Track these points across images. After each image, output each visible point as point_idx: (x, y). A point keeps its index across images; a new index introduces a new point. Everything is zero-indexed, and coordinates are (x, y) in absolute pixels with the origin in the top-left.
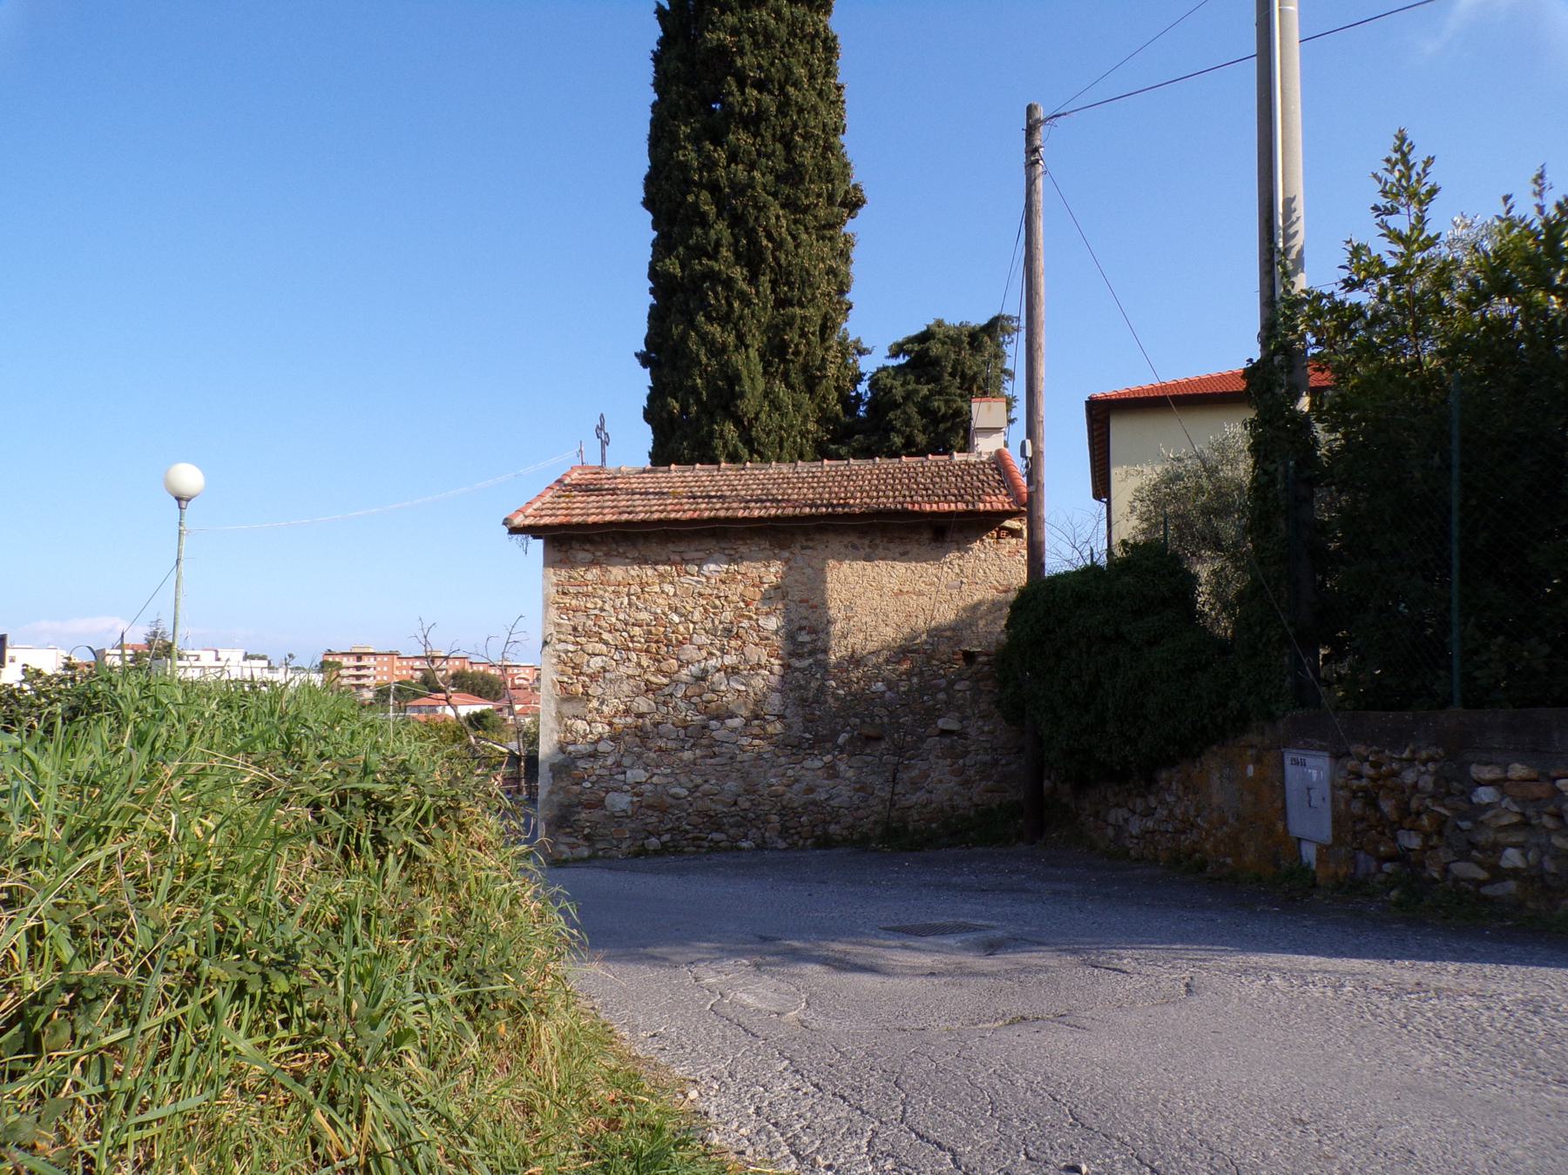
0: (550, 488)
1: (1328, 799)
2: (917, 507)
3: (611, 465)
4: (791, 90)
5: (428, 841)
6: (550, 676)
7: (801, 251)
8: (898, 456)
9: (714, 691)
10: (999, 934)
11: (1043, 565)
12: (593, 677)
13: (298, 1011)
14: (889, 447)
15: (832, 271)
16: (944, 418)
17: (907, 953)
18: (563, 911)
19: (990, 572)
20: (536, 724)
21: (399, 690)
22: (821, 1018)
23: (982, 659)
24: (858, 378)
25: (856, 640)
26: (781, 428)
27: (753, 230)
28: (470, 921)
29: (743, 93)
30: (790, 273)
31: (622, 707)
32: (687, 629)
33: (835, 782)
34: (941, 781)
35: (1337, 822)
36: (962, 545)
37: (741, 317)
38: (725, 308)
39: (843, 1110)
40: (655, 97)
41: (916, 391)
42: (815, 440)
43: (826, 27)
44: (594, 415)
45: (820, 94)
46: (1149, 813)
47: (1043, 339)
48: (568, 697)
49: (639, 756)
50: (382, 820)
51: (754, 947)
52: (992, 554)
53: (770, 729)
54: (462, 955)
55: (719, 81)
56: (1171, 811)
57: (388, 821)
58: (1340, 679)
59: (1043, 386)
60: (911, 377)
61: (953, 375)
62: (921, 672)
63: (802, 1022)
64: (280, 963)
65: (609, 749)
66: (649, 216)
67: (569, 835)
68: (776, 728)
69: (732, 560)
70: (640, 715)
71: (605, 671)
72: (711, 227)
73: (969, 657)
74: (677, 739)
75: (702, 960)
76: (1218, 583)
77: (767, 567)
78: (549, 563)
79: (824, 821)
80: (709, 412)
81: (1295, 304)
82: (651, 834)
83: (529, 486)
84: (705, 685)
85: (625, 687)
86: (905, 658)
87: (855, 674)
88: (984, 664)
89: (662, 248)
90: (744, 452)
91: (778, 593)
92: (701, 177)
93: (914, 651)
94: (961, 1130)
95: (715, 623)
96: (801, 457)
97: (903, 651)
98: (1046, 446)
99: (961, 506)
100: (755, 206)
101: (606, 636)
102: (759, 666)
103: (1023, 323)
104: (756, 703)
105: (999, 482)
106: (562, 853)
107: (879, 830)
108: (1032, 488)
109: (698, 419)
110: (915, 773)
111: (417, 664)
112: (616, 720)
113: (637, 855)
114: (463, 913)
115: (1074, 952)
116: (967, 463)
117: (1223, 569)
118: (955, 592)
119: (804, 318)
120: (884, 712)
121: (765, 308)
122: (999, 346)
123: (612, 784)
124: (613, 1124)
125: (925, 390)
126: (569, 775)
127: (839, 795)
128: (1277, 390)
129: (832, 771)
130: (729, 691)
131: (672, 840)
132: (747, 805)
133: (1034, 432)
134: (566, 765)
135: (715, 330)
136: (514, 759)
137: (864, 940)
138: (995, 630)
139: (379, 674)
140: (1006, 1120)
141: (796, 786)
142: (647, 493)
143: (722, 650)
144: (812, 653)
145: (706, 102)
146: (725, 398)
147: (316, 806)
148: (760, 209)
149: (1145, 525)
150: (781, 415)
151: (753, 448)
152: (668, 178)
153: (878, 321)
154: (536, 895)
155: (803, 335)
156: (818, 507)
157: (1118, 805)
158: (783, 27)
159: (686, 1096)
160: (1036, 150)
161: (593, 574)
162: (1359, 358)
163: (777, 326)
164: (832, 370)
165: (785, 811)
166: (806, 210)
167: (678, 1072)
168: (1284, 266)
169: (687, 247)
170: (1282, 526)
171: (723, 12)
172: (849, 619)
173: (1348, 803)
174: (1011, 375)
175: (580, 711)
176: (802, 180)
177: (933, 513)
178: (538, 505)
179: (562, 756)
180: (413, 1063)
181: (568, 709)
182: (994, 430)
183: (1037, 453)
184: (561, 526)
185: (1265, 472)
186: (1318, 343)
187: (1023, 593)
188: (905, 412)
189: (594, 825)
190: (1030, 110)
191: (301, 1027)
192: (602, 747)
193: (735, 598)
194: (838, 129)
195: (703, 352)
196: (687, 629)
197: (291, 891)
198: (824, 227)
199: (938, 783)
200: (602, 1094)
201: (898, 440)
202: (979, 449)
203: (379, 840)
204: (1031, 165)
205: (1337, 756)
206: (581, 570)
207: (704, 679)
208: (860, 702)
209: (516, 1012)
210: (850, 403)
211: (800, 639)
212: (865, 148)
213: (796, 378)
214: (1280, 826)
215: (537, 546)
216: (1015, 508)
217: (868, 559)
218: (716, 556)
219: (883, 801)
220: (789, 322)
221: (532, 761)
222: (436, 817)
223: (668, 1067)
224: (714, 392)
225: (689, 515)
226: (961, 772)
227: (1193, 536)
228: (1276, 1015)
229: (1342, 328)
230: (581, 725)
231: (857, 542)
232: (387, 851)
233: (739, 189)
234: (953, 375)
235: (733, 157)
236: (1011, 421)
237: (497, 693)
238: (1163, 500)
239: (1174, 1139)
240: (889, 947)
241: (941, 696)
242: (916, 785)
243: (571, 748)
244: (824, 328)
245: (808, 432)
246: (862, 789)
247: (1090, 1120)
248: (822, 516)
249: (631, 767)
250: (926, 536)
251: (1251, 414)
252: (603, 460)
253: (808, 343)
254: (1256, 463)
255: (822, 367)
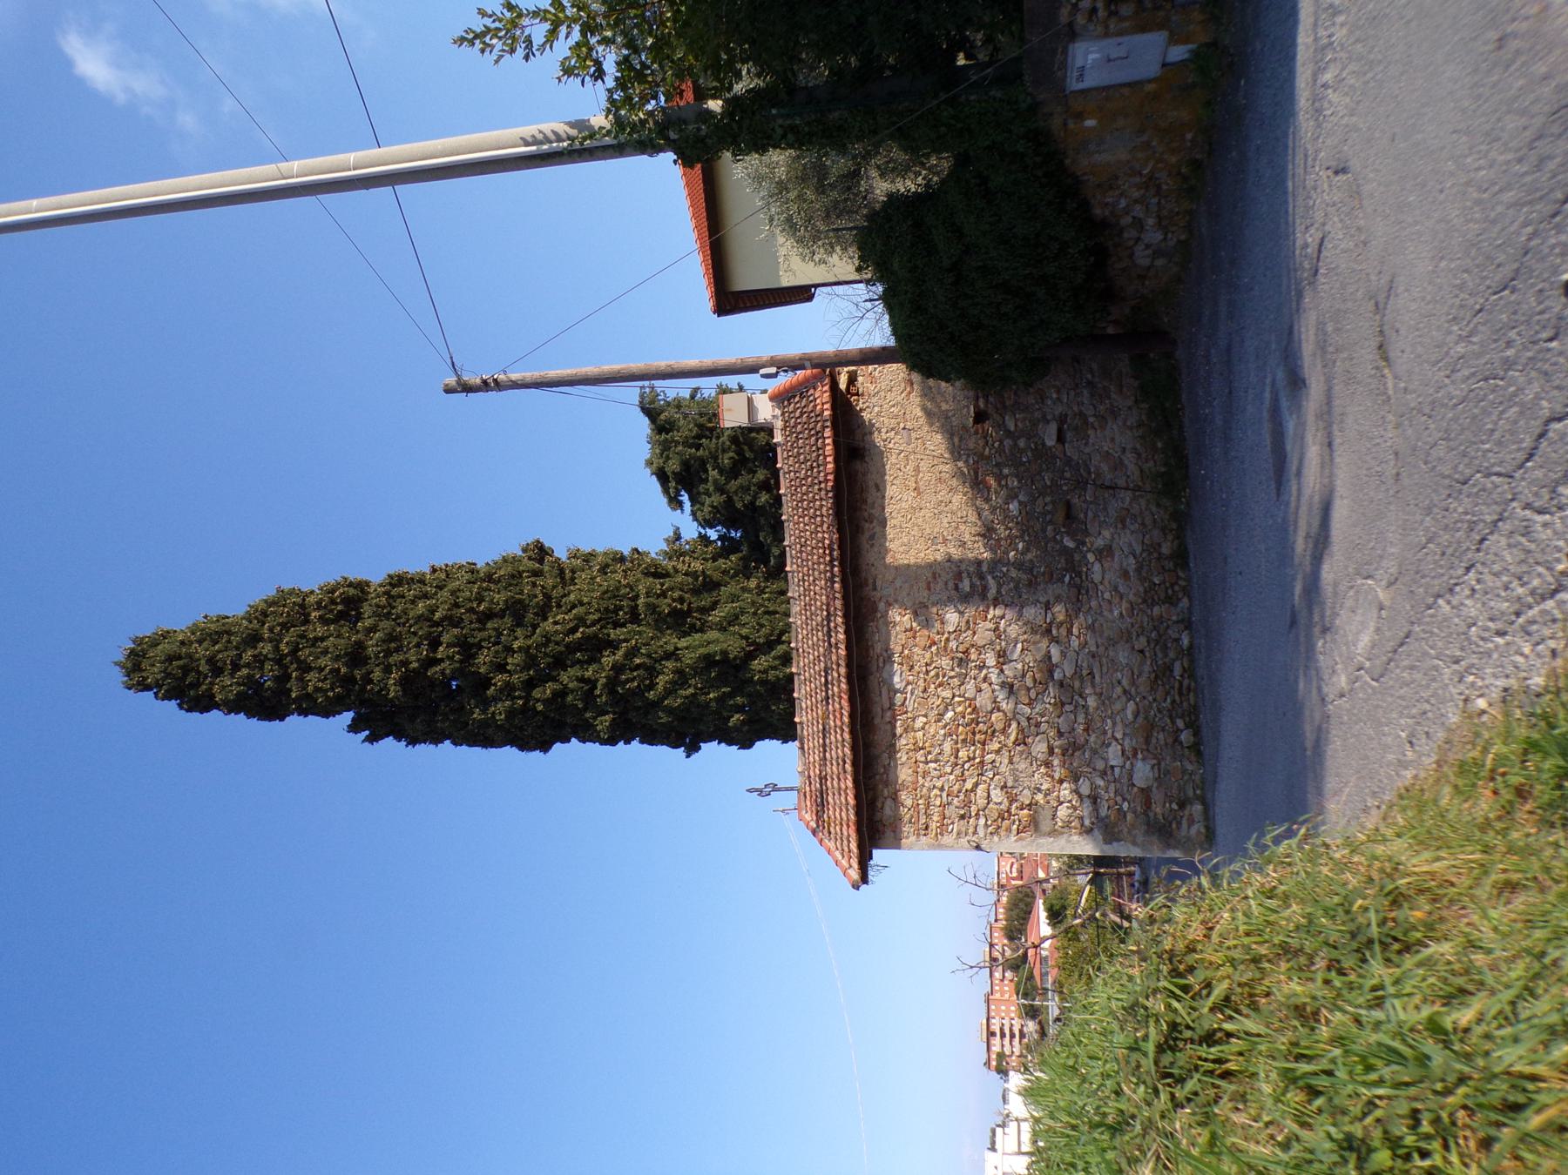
0: (821, 841)
1: (1120, 39)
2: (831, 477)
3: (797, 781)
4: (438, 615)
5: (1208, 985)
6: (1011, 843)
7: (586, 600)
8: (779, 497)
9: (1024, 676)
10: (1281, 374)
11: (884, 349)
12: (1012, 800)
13: (1410, 1140)
14: (771, 506)
15: (603, 570)
16: (740, 453)
17: (1305, 472)
18: (1277, 841)
19: (893, 402)
20: (1058, 857)
21: (1025, 996)
22: (1384, 563)
23: (981, 404)
24: (704, 539)
25: (967, 532)
26: (755, 614)
27: (567, 646)
28: (1295, 943)
29: (442, 660)
30: (606, 609)
31: (1043, 770)
32: (959, 703)
33: (1115, 550)
34: (1113, 440)
35: (1143, 29)
36: (866, 430)
37: (649, 656)
38: (641, 672)
39: (1497, 541)
40: (447, 742)
41: (715, 482)
42: (766, 580)
43: (381, 585)
44: (747, 799)
45: (440, 588)
46: (1139, 224)
47: (662, 364)
48: (1033, 825)
49: (1094, 752)
50: (1188, 1034)
51: (1303, 634)
52: (874, 400)
53: (1061, 617)
54: (1335, 954)
55: (432, 683)
56: (1136, 201)
57: (1188, 1027)
58: (988, 40)
59: (708, 361)
60: (702, 488)
61: (698, 447)
62: (997, 465)
63: (1390, 584)
64: (1359, 1158)
65: (1087, 783)
66: (557, 746)
67: (1179, 824)
68: (1059, 611)
69: (889, 660)
70: (1051, 751)
71: (1005, 786)
72: (566, 686)
73: (980, 417)
74: (1074, 712)
75: (1319, 689)
76: (893, 170)
77: (895, 624)
78: (896, 844)
79: (1158, 559)
80: (742, 685)
81: (620, 124)
82: (1176, 740)
83: (820, 864)
84: (1017, 684)
85: (1022, 766)
86: (984, 482)
87: (1002, 532)
88: (987, 401)
89: (587, 734)
90: (781, 649)
91: (920, 612)
92: (520, 698)
93: (976, 473)
94: (1521, 413)
95: (953, 675)
96: (783, 592)
97: (976, 484)
98: (765, 353)
99: (828, 432)
100: (545, 645)
101: (969, 785)
102: (996, 629)
103: (646, 383)
104: (1034, 632)
105: (802, 398)
106: (1199, 832)
107: (1166, 502)
108: (807, 364)
109: (749, 695)
110: (1105, 467)
111: (998, 975)
112: (1057, 776)
113: (1199, 754)
114: (1286, 951)
115: (1300, 295)
116: (784, 429)
117: (878, 167)
118: (913, 435)
119: (648, 595)
120: (1040, 501)
121: (640, 633)
122: (668, 404)
123: (1125, 780)
124: (1521, 793)
125: (713, 474)
126: (1116, 824)
127: (1130, 545)
128: (703, 133)
129: (1105, 553)
130: (1022, 660)
131: (1182, 717)
132: (1143, 640)
133: (751, 364)
134: (1105, 828)
135: (661, 681)
136: (1096, 881)
137: (1292, 518)
138: (952, 394)
139: (1009, 1013)
140: (1509, 364)
141: (1121, 589)
142: (824, 745)
143: (981, 668)
144: (982, 577)
145: (450, 695)
146: (727, 669)
147: (1177, 1105)
148: (548, 641)
149: (838, 249)
150: (743, 613)
151: (776, 641)
152: (521, 729)
153: (636, 517)
154: (1260, 869)
155: (663, 594)
156: (833, 575)
157: (1131, 256)
158: (382, 625)
159: (1484, 712)
160: (485, 382)
161: (906, 798)
162: (668, 57)
163: (656, 621)
164: (697, 566)
165: (1149, 599)
166: (548, 597)
167: (1454, 719)
168: (585, 139)
169: (585, 709)
170: (836, 114)
171: (371, 681)
172: (945, 540)
173: (1122, 19)
174: (696, 390)
175: (1048, 813)
176: (520, 601)
177: (836, 461)
178: (838, 854)
179: (1096, 832)
180: (1465, 1016)
181: (1046, 825)
182: (752, 404)
183: (773, 362)
184: (859, 831)
185: (784, 136)
186: (655, 97)
187: (912, 367)
188: (736, 492)
189: (1169, 798)
190: (449, 390)
191: (1428, 1137)
192: (1085, 790)
193: (928, 655)
194: (472, 569)
195: (682, 692)
196: (959, 703)
197: (1272, 1137)
198: (563, 578)
199: (1115, 442)
200: (1485, 805)
201: (764, 498)
202: (769, 417)
203: (1209, 1039)
204: (498, 386)
205: (1072, 34)
206: (903, 811)
207: (1012, 686)
208: (1029, 526)
209: (1397, 899)
210: (729, 547)
211: (967, 589)
212: (488, 543)
213: (706, 601)
214: (1150, 87)
215: (879, 855)
216: (828, 382)
217: (883, 523)
218: (885, 675)
219: (1134, 499)
220: (652, 608)
221: (1099, 861)
222: (1180, 975)
223: (1450, 730)
224: (721, 680)
225: (845, 704)
226: (1102, 419)
227: (846, 200)
228: (1370, 75)
229: (640, 77)
230: (1063, 812)
231: (867, 535)
232: (1221, 1029)
233: (531, 662)
234: (698, 447)
235: (501, 668)
236: (741, 389)
237: (1027, 895)
238: (809, 235)
239: (1528, 179)
240: (1299, 490)
241: (1022, 443)
242: (1118, 465)
243: (1087, 822)
244: (656, 575)
245: (758, 586)
246: (1123, 521)
247: (1507, 271)
248: (843, 571)
249: (1106, 760)
250: (858, 466)
251: (727, 155)
252: (792, 789)
253: (672, 589)
254: (775, 147)
255: (695, 575)
